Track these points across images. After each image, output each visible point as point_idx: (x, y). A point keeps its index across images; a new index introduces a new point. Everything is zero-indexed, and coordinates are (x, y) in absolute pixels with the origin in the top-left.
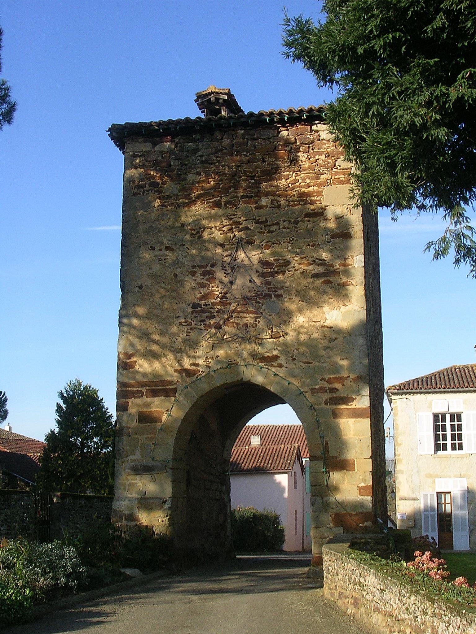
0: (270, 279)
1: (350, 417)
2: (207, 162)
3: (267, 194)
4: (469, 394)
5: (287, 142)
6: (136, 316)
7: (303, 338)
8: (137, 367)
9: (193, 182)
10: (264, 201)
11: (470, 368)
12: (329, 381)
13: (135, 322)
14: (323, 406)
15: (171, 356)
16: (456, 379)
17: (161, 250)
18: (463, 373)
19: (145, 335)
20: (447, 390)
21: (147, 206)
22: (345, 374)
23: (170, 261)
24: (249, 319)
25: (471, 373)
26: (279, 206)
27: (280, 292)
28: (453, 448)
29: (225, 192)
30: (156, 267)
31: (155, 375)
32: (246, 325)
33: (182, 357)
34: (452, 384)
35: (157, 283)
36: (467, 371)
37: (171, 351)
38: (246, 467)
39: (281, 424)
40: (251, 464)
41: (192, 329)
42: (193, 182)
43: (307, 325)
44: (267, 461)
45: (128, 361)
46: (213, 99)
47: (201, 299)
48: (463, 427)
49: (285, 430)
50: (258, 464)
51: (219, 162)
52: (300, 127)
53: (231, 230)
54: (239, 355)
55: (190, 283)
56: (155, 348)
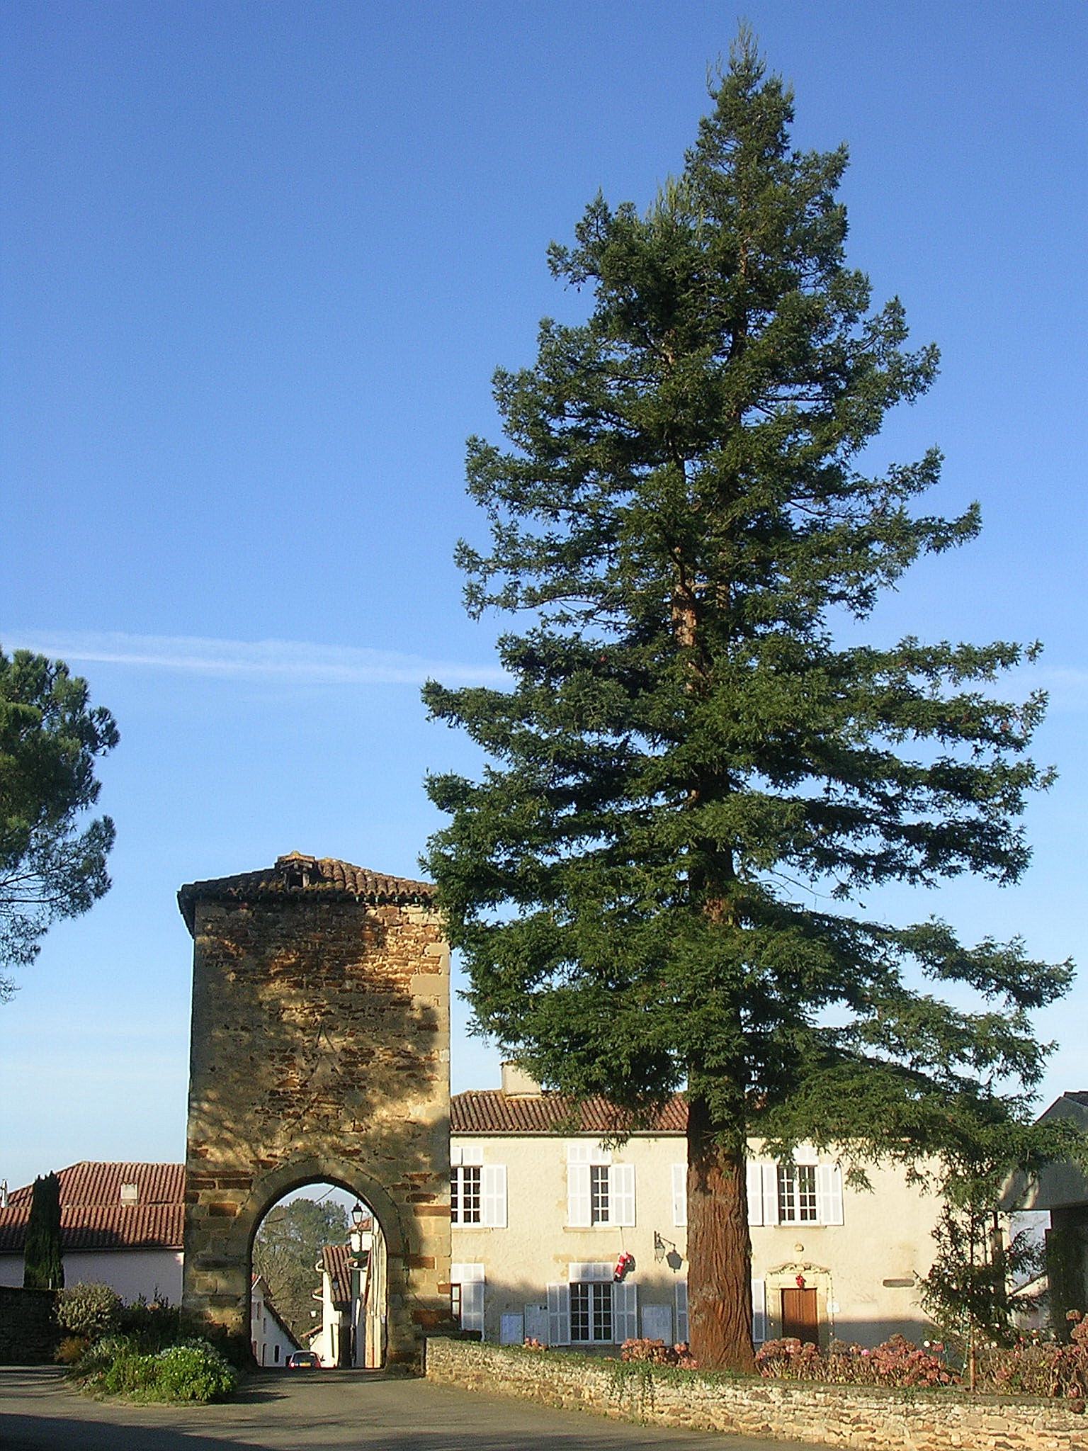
0: (354, 1069)
1: (431, 1215)
2: (289, 936)
3: (351, 978)
4: (492, 1139)
5: (374, 922)
6: (208, 1100)
7: (385, 1132)
8: (208, 1156)
9: (273, 957)
10: (348, 985)
11: (493, 1097)
12: (411, 1178)
13: (206, 1106)
14: (404, 1202)
15: (245, 1146)
16: (473, 1115)
17: (236, 1030)
18: (483, 1105)
19: (217, 1122)
20: (461, 1132)
21: (221, 979)
22: (426, 1171)
23: (246, 1042)
24: (328, 1109)
25: (495, 1106)
26: (364, 992)
27: (363, 1083)
28: (467, 1219)
29: (307, 971)
30: (231, 1049)
31: (227, 1164)
32: (327, 1116)
33: (258, 1147)
34: (469, 1123)
35: (232, 1066)
36: (488, 1101)
37: (247, 1140)
38: (131, 1239)
39: (160, 1163)
40: (138, 1235)
41: (269, 1118)
42: (273, 957)
43: (390, 1119)
44: (163, 1231)
45: (199, 1149)
46: (296, 866)
47: (279, 1086)
48: (481, 1188)
49: (170, 1174)
50: (151, 1235)
51: (301, 937)
52: (389, 907)
53: (312, 1013)
54: (318, 1147)
55: (266, 1067)
56: (228, 1135)
